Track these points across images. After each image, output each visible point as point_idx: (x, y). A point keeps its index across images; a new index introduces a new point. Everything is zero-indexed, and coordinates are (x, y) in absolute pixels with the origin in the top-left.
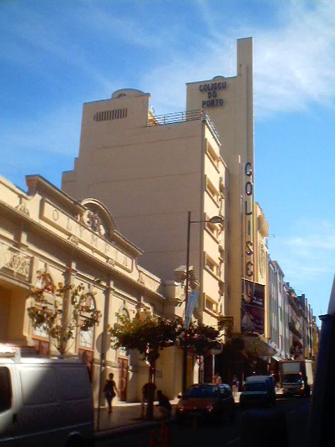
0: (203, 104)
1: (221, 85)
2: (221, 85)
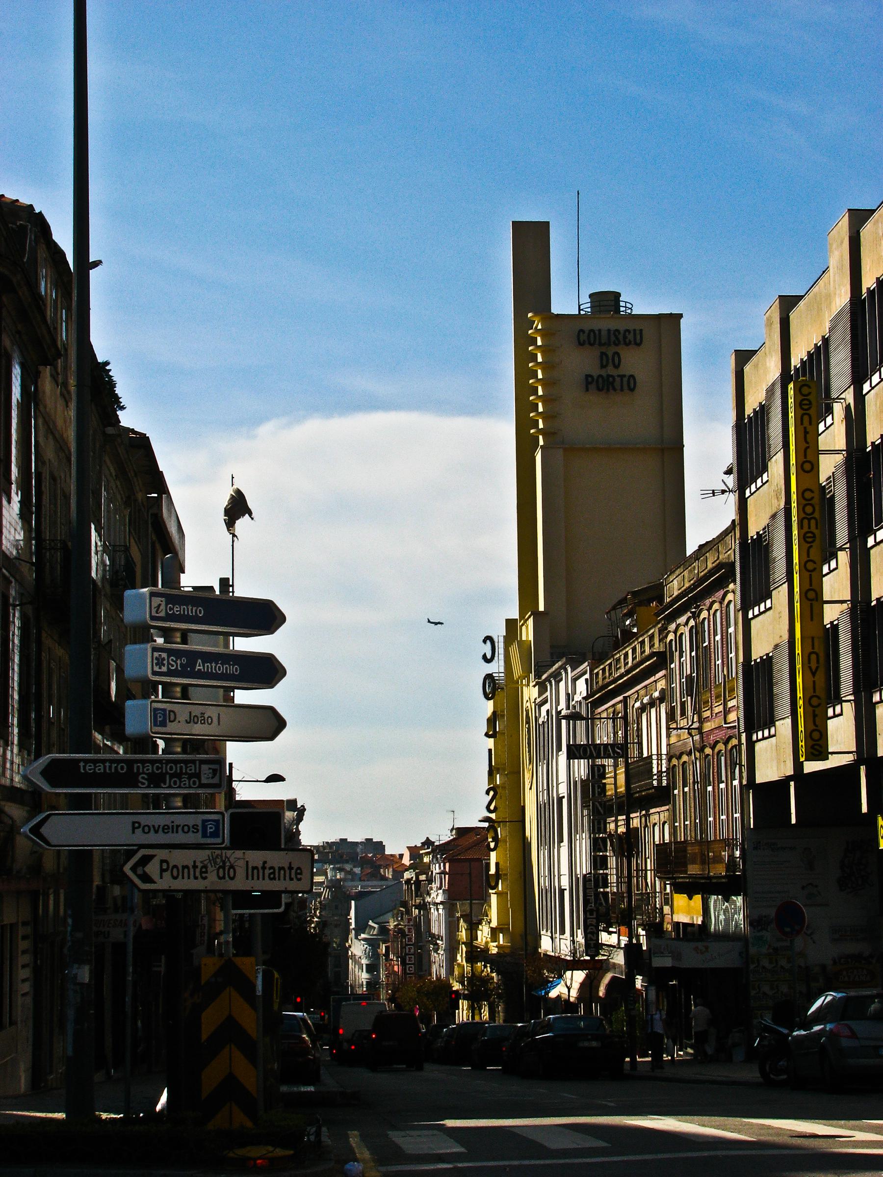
1: (630, 337)
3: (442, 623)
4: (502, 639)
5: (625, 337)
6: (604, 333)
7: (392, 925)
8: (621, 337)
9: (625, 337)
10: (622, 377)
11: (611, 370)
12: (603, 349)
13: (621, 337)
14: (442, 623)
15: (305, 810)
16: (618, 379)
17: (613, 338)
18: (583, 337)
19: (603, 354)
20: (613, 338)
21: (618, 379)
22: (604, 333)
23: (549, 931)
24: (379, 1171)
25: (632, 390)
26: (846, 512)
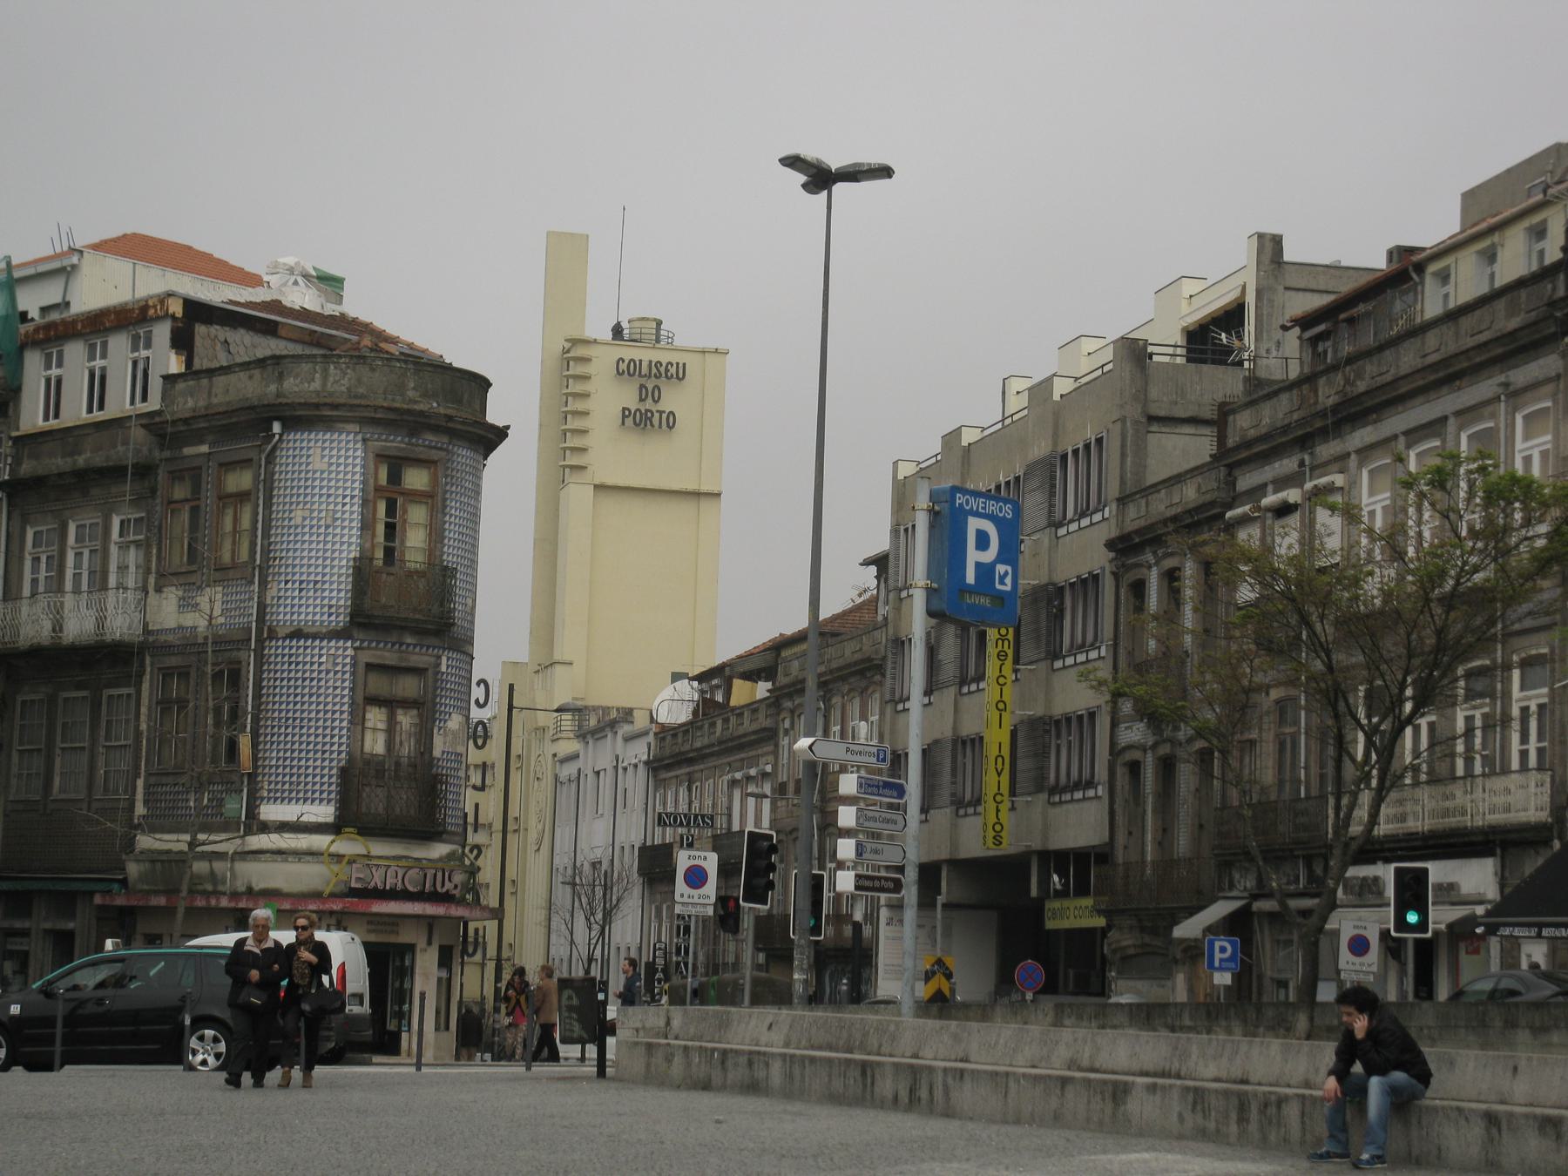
0: (624, 417)
1: (673, 370)
2: (673, 370)
3: (885, 172)
4: (497, 683)
5: (667, 370)
6: (645, 365)
7: (507, 1021)
8: (662, 370)
9: (667, 370)
10: (661, 413)
11: (649, 404)
12: (643, 381)
13: (662, 370)
14: (885, 172)
15: (890, 176)
16: (657, 415)
17: (654, 370)
18: (623, 366)
19: (642, 386)
20: (654, 370)
21: (657, 415)
22: (645, 365)
23: (471, 932)
24: (150, 451)
25: (670, 428)
26: (286, 835)
